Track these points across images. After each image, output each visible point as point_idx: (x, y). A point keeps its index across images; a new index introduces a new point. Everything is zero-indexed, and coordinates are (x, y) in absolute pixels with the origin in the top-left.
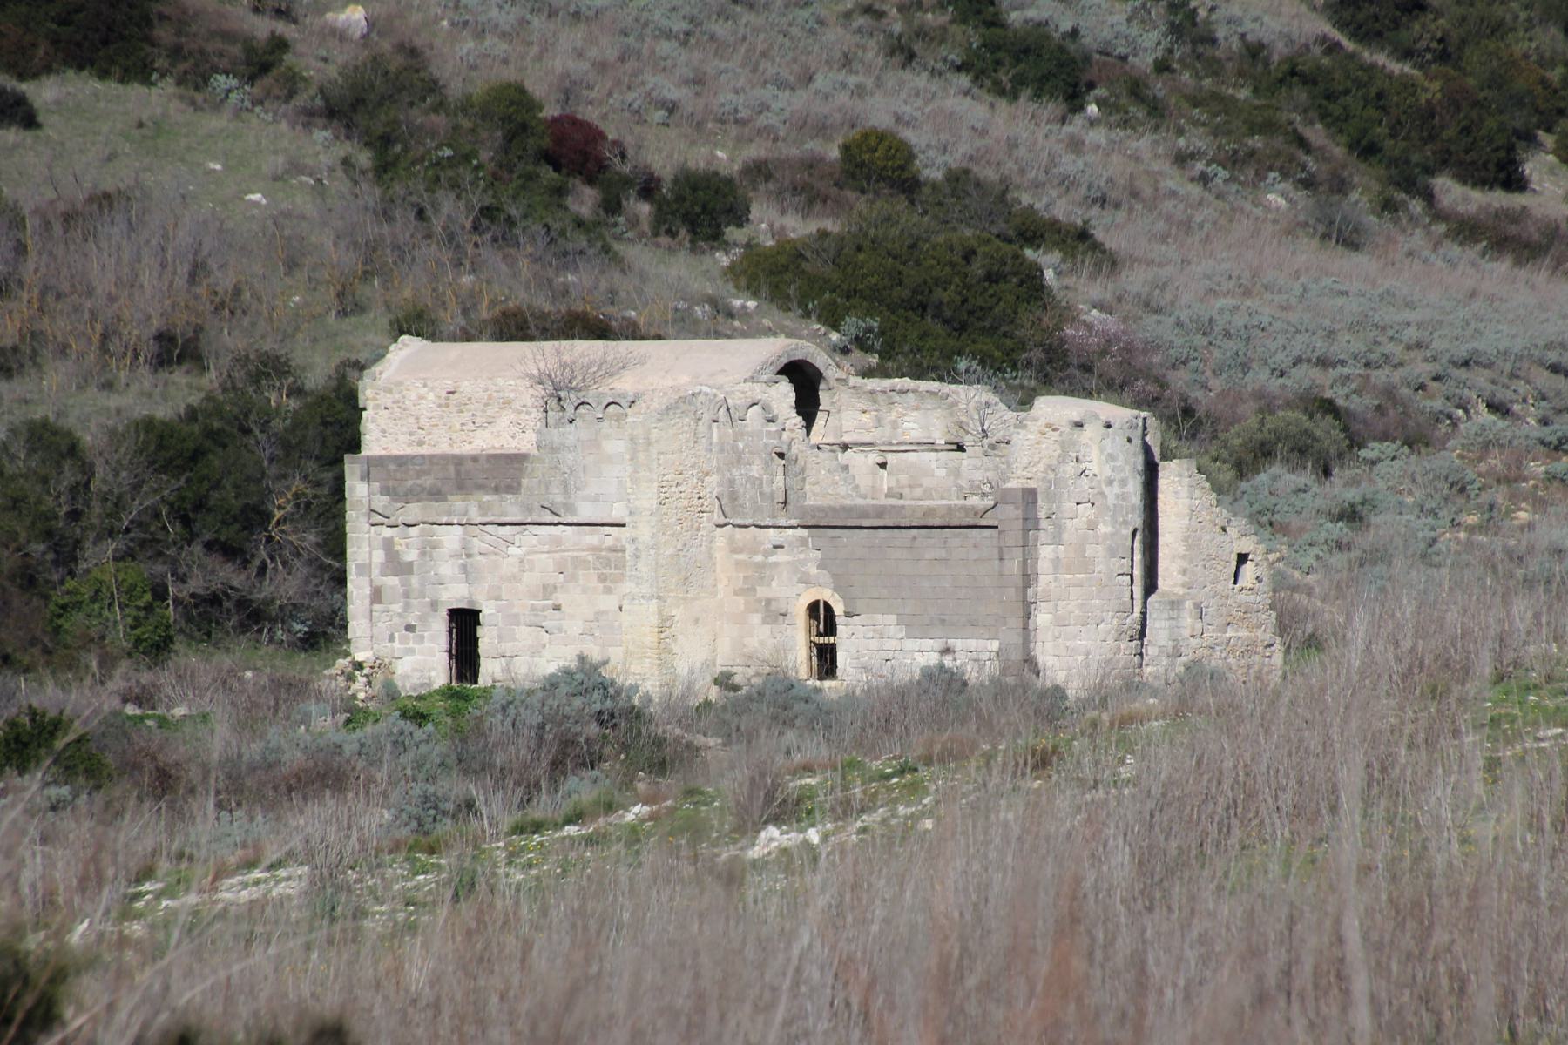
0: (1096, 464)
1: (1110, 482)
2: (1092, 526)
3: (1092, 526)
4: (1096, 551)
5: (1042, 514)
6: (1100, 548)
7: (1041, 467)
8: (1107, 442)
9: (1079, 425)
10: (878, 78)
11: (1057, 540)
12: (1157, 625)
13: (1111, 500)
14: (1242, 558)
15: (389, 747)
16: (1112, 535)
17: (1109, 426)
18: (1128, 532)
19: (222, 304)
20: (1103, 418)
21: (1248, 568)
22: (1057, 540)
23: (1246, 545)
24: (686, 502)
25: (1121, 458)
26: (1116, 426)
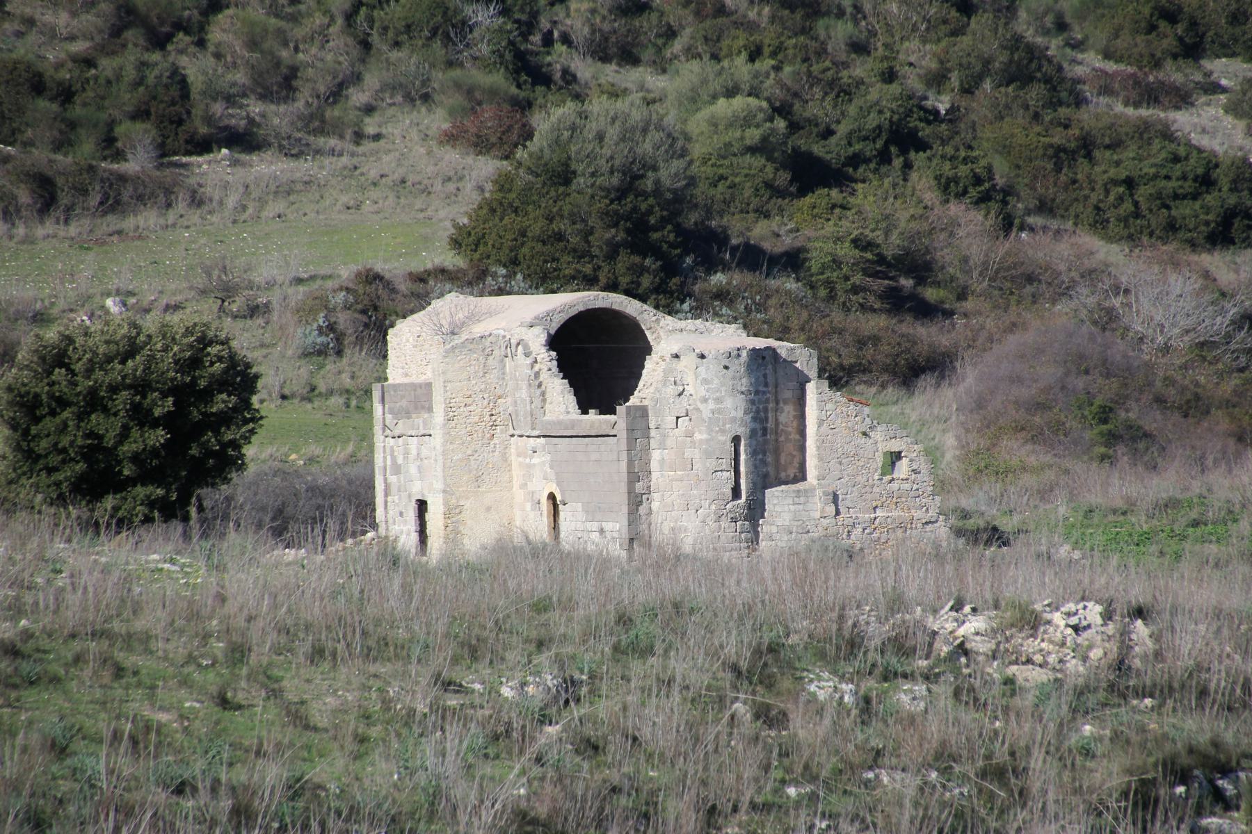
0: (693, 388)
1: (705, 400)
2: (690, 435)
3: (690, 435)
4: (696, 454)
5: (652, 425)
6: (697, 451)
7: (652, 389)
8: (702, 370)
9: (677, 356)
10: (332, 496)
11: (662, 446)
12: (778, 509)
13: (706, 414)
14: (896, 457)
15: (857, 102)
16: (707, 441)
17: (702, 357)
18: (727, 439)
19: (473, 108)
20: (697, 351)
21: (903, 468)
22: (662, 446)
23: (895, 446)
24: (476, 419)
25: (716, 381)
26: (710, 357)
